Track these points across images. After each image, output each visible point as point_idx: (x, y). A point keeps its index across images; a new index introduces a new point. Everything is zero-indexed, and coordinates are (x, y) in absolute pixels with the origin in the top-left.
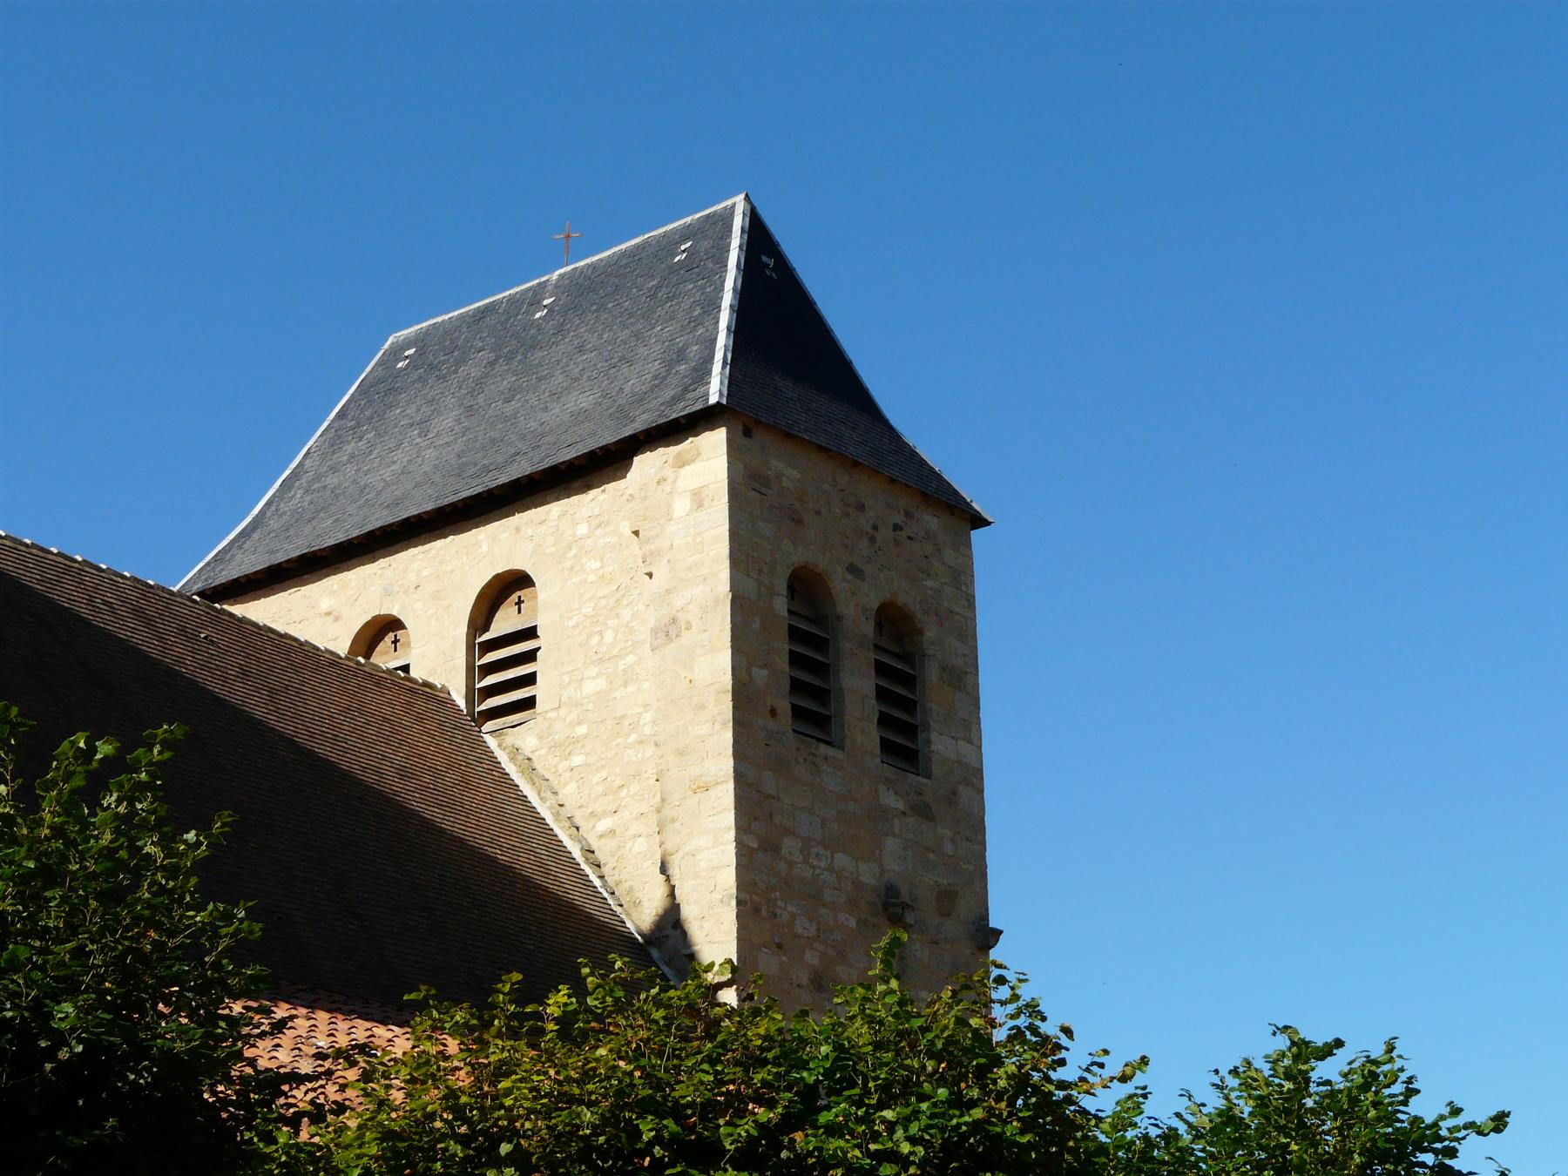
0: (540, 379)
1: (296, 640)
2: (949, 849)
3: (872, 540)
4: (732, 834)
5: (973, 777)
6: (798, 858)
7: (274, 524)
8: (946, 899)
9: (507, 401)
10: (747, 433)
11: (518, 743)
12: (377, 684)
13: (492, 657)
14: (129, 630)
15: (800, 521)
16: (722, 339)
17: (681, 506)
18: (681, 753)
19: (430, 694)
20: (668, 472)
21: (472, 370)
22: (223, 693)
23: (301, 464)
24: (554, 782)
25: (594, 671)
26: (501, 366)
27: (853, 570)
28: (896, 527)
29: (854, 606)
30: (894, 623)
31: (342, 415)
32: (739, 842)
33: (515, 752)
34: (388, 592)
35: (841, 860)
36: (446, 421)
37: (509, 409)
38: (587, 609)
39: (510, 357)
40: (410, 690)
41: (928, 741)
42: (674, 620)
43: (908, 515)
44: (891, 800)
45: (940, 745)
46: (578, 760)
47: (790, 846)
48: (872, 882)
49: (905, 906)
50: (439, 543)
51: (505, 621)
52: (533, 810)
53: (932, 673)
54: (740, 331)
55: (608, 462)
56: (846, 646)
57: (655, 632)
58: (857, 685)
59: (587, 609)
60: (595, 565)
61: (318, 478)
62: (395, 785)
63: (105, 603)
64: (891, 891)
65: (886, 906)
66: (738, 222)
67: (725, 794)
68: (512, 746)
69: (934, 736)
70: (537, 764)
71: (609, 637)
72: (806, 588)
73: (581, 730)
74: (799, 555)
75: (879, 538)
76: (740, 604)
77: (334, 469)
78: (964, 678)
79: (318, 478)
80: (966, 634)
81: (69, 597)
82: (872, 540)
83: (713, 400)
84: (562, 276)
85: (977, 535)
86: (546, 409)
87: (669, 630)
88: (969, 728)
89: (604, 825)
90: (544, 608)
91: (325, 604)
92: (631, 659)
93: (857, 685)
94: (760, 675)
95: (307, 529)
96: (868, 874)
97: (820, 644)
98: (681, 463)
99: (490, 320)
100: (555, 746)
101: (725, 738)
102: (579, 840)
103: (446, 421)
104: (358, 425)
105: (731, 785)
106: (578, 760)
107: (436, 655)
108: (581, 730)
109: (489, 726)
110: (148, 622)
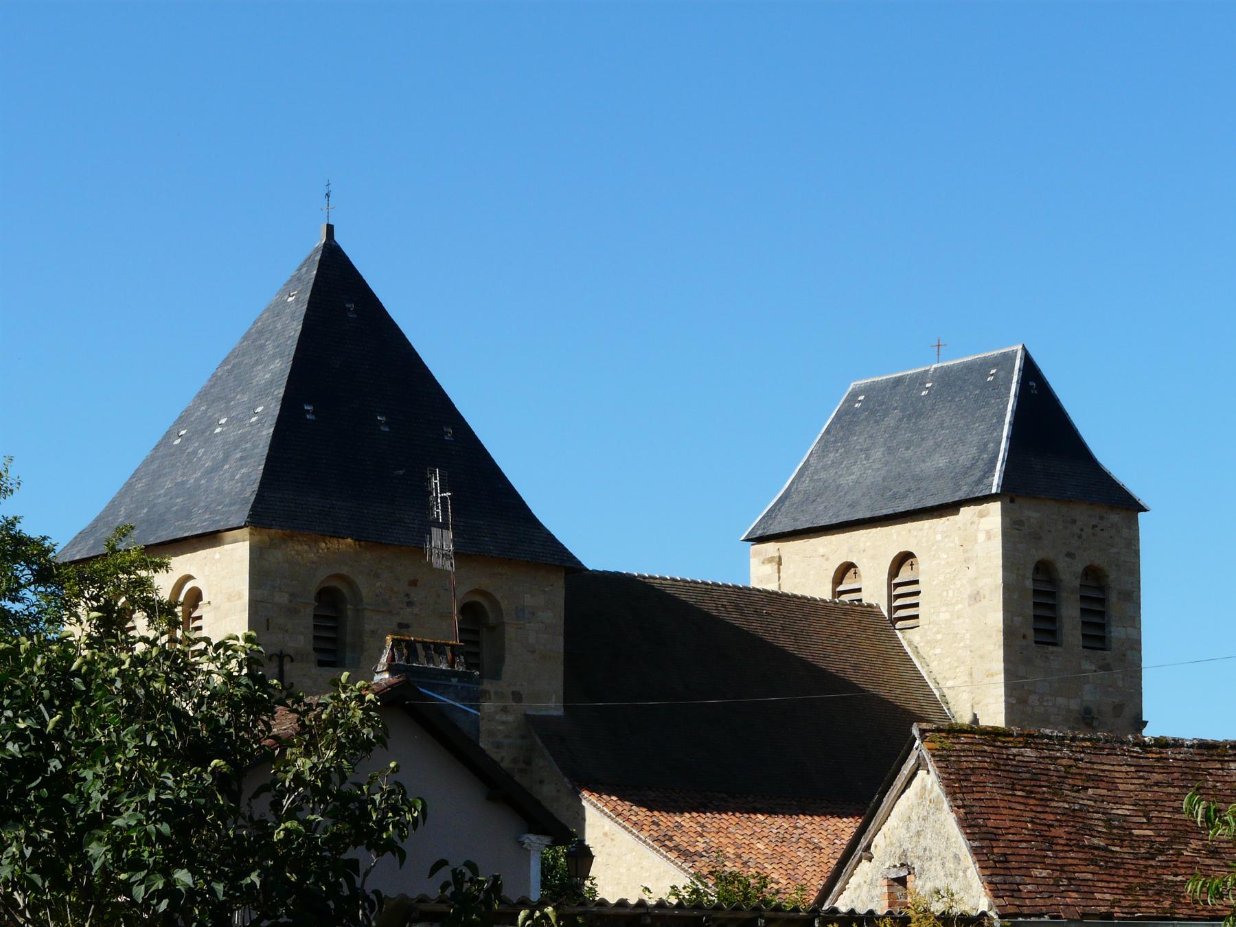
0: (923, 439)
1: (805, 598)
2: (1120, 684)
3: (1080, 537)
4: (1003, 698)
5: (1136, 645)
6: (1037, 703)
7: (796, 498)
8: (1118, 709)
9: (907, 449)
10: (1012, 501)
11: (912, 638)
12: (845, 614)
13: (899, 602)
14: (734, 618)
15: (1040, 538)
16: (1004, 444)
17: (981, 537)
18: (981, 657)
19: (872, 610)
20: (976, 519)
21: (890, 421)
22: (775, 642)
23: (808, 460)
24: (927, 660)
25: (944, 609)
26: (904, 425)
27: (1070, 555)
28: (1094, 527)
29: (1069, 573)
30: (1094, 578)
31: (828, 431)
32: (1006, 702)
33: (910, 643)
34: (850, 550)
35: (1060, 700)
36: (878, 453)
37: (909, 454)
38: (941, 578)
39: (909, 418)
40: (861, 612)
41: (1110, 632)
42: (978, 593)
43: (1101, 518)
44: (1086, 665)
45: (1117, 632)
46: (938, 651)
47: (1033, 699)
48: (1076, 708)
49: (1093, 718)
50: (874, 530)
51: (905, 574)
52: (918, 672)
53: (1113, 597)
54: (1013, 438)
55: (949, 508)
56: (1064, 595)
57: (970, 597)
58: (1070, 613)
59: (941, 578)
60: (945, 556)
61: (816, 472)
62: (852, 676)
63: (723, 606)
64: (1088, 711)
65: (1084, 719)
66: (1018, 364)
67: (1000, 678)
68: (909, 639)
69: (1113, 629)
70: (920, 650)
71: (951, 593)
72: (1044, 570)
73: (939, 637)
74: (1038, 555)
75: (1084, 535)
76: (1009, 589)
77: (824, 468)
78: (1132, 597)
79: (816, 472)
80: (1134, 571)
81: (709, 607)
82: (1080, 537)
83: (994, 491)
84: (936, 369)
85: (1141, 515)
86: (924, 461)
87: (976, 597)
88: (1134, 620)
89: (950, 683)
90: (925, 570)
91: (822, 551)
92: (960, 606)
93: (1070, 613)
94: (1018, 620)
95: (811, 508)
96: (1074, 705)
97: (1052, 595)
98: (981, 515)
99: (900, 389)
100: (928, 642)
101: (1000, 653)
102: (939, 689)
103: (878, 453)
104: (836, 442)
105: (1002, 676)
106: (938, 651)
107: (873, 589)
108: (939, 637)
109: (899, 625)
110: (742, 613)
